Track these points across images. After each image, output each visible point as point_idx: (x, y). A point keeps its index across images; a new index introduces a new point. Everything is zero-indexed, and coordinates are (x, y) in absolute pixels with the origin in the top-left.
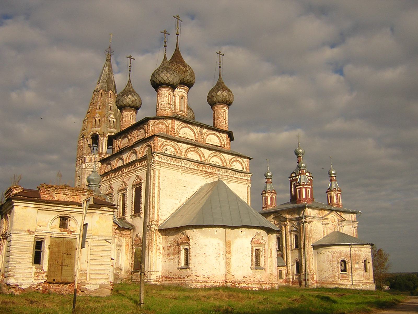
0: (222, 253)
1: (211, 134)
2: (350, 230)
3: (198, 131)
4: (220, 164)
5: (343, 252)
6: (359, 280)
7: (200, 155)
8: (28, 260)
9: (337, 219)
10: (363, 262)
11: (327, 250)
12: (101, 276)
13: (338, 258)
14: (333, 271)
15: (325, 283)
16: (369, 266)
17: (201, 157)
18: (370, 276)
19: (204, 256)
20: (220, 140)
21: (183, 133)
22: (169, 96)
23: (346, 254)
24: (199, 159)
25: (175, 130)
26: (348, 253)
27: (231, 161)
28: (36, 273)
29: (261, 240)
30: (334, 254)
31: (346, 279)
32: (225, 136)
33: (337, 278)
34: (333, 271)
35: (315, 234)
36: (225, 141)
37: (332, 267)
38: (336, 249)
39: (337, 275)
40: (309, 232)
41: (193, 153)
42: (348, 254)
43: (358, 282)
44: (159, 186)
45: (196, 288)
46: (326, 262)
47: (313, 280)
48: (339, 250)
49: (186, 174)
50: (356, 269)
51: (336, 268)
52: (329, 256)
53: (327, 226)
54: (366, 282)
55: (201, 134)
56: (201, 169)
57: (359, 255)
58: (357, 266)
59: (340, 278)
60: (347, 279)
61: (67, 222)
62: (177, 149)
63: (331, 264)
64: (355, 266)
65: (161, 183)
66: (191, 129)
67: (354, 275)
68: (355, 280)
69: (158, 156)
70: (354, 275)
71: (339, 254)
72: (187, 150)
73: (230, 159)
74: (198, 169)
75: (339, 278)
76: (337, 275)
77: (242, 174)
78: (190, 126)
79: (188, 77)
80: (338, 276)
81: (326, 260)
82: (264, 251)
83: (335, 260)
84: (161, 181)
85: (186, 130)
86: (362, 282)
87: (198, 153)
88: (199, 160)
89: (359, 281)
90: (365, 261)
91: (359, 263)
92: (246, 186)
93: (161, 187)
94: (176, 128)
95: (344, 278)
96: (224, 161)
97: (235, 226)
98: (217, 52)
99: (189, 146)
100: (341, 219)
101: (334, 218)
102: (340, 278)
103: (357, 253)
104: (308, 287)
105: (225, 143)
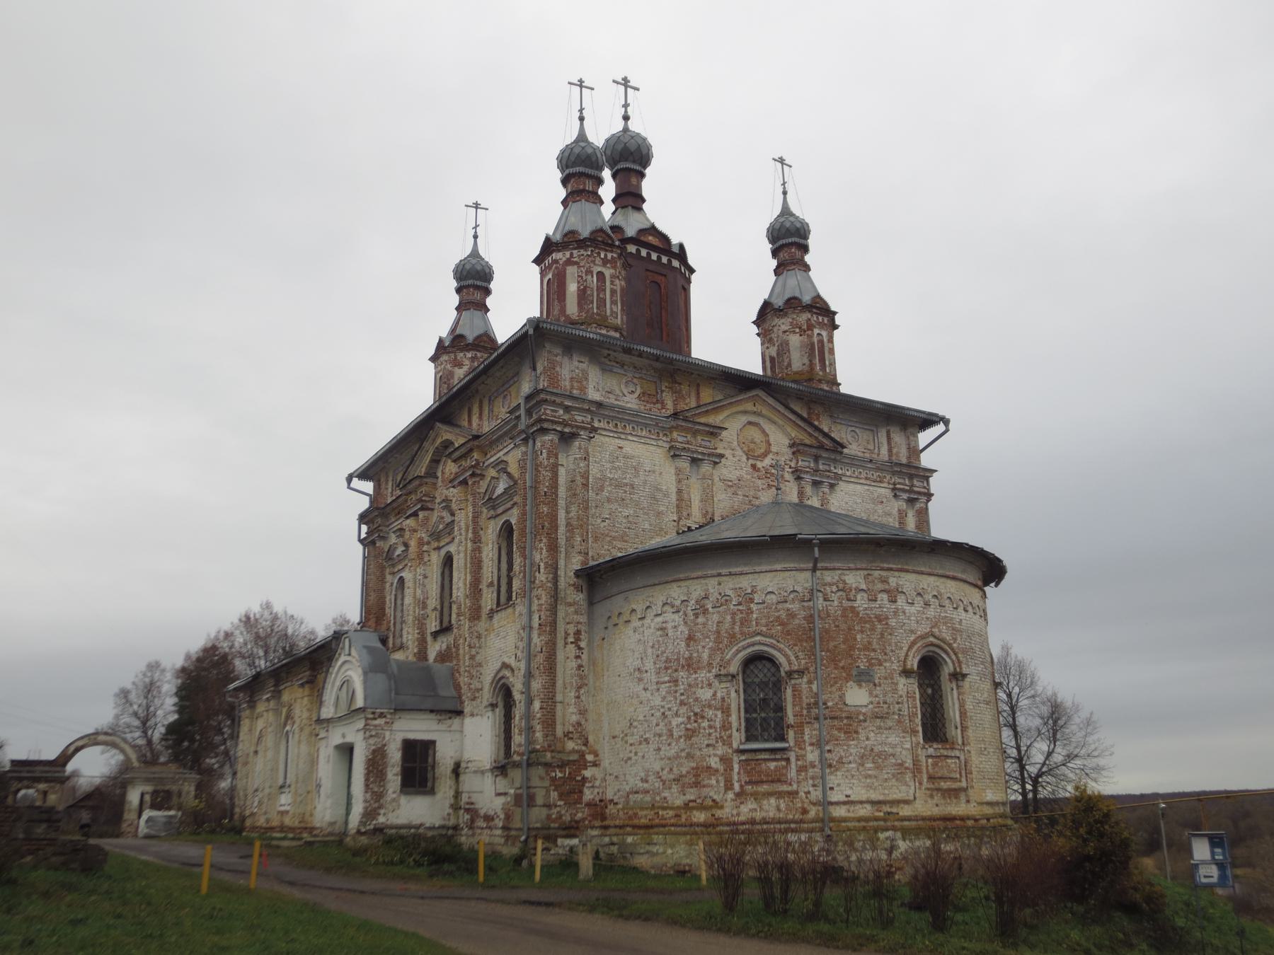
2: (880, 509)
5: (757, 598)
6: (875, 796)
9: (787, 442)
10: (906, 673)
11: (659, 597)
13: (723, 640)
14: (690, 734)
15: (643, 821)
16: (962, 706)
18: (969, 772)
23: (783, 615)
26: (794, 607)
30: (701, 620)
31: (780, 795)
34: (694, 731)
35: (614, 506)
37: (683, 710)
39: (714, 762)
40: (562, 492)
42: (792, 615)
43: (865, 811)
47: (579, 801)
48: (729, 586)
50: (849, 723)
51: (710, 713)
52: (670, 633)
54: (936, 811)
57: (880, 619)
58: (857, 697)
59: (737, 787)
60: (785, 788)
61: (391, 827)
63: (681, 688)
64: (842, 697)
67: (840, 761)
70: (840, 761)
71: (734, 614)
75: (729, 786)
77: (1013, 740)
80: (721, 768)
81: (649, 665)
83: (705, 656)
86: (905, 811)
89: (873, 803)
90: (929, 668)
91: (879, 673)
95: (764, 788)
100: (814, 442)
101: (764, 432)
102: (737, 787)
103: (861, 602)
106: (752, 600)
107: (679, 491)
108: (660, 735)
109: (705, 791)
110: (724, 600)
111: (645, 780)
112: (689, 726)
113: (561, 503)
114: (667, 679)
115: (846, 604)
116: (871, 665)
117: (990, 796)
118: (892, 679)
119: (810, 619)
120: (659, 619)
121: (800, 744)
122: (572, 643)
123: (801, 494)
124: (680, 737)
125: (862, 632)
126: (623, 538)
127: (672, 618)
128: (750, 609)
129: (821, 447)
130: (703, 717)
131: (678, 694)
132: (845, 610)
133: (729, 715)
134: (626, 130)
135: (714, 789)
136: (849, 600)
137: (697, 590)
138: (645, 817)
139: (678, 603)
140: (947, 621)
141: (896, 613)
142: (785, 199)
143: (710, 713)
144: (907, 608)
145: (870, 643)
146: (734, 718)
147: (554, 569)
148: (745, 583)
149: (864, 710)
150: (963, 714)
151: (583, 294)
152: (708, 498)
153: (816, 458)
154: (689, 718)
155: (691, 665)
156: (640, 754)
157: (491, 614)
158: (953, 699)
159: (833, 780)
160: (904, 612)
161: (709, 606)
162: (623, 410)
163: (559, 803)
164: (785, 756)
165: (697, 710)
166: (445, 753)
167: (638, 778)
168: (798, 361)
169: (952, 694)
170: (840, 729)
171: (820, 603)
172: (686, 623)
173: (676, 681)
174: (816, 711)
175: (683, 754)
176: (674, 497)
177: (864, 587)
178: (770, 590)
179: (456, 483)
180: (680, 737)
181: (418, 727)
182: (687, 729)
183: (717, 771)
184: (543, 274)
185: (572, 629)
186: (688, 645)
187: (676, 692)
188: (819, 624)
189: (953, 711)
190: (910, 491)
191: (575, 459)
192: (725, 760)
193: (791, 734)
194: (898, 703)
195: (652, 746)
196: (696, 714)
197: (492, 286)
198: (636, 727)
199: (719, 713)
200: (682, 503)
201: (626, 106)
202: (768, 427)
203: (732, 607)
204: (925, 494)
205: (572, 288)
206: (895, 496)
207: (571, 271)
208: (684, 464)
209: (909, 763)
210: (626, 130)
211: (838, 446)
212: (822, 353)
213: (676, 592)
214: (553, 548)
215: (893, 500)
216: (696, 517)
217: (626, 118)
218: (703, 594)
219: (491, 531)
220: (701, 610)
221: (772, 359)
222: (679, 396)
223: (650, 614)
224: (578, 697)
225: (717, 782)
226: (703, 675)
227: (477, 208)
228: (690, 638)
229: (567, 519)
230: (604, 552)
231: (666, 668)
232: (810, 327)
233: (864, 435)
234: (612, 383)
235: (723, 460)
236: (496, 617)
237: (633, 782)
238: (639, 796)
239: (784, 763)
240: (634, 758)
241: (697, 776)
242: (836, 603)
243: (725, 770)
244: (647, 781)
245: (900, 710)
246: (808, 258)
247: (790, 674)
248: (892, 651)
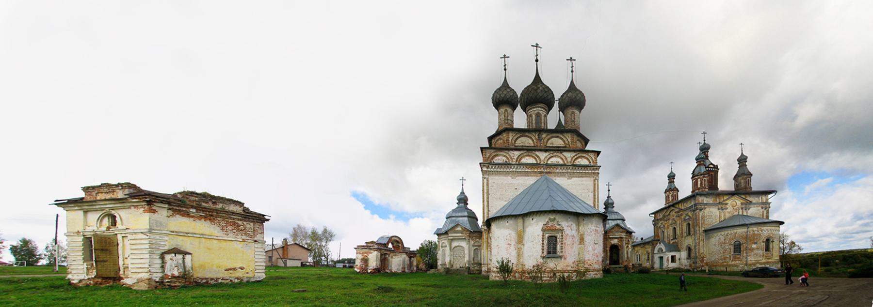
0: (513, 243)
1: (552, 137)
2: (758, 211)
3: (537, 137)
4: (561, 162)
6: (756, 260)
7: (535, 158)
8: (79, 258)
10: (763, 242)
11: (719, 234)
12: (141, 270)
14: (724, 253)
17: (536, 160)
19: (497, 248)
20: (564, 142)
21: (520, 142)
22: (506, 112)
24: (535, 162)
25: (510, 141)
27: (574, 159)
28: (88, 269)
29: (556, 225)
32: (570, 136)
33: (728, 260)
36: (570, 141)
38: (729, 232)
39: (728, 256)
40: (700, 218)
41: (527, 158)
43: (754, 262)
44: (483, 192)
45: (644, 271)
46: (717, 246)
48: (732, 232)
49: (517, 178)
50: (752, 250)
53: (724, 210)
55: (540, 139)
56: (536, 170)
58: (754, 246)
62: (508, 157)
65: (490, 190)
66: (529, 137)
67: (750, 255)
68: (751, 261)
69: (485, 166)
72: (519, 156)
73: (572, 156)
74: (532, 170)
75: (730, 259)
76: (728, 256)
78: (527, 134)
79: (540, 94)
82: (561, 237)
84: (490, 188)
85: (523, 139)
87: (533, 157)
88: (535, 162)
90: (768, 240)
91: (758, 242)
92: (593, 179)
93: (490, 193)
94: (510, 139)
96: (564, 159)
97: (523, 214)
98: (533, 45)
99: (522, 152)
103: (756, 232)
104: (488, 277)
105: (570, 143)
117: (776, 258)
119: (747, 235)
121: (743, 253)
123: (742, 212)
126: (710, 224)
127: (721, 237)
129: (747, 203)
134: (705, 143)
135: (728, 260)
137: (726, 232)
138: (715, 264)
146: (732, 250)
147: (699, 230)
148: (735, 231)
150: (773, 247)
151: (701, 183)
152: (725, 215)
153: (746, 205)
155: (724, 243)
157: (685, 237)
159: (748, 258)
162: (710, 204)
166: (677, 257)
168: (743, 185)
171: (749, 233)
173: (722, 246)
174: (747, 249)
176: (719, 216)
181: (673, 254)
184: (693, 181)
188: (748, 236)
189: (771, 246)
192: (730, 256)
193: (742, 252)
200: (720, 217)
201: (704, 138)
202: (736, 201)
204: (750, 175)
205: (699, 183)
207: (699, 180)
209: (762, 255)
210: (705, 143)
211: (751, 202)
212: (748, 182)
213: (723, 233)
214: (699, 227)
216: (723, 219)
217: (704, 140)
219: (685, 225)
221: (737, 185)
222: (720, 199)
226: (727, 245)
227: (537, 47)
228: (725, 239)
230: (707, 227)
232: (746, 178)
233: (756, 199)
234: (708, 199)
236: (687, 238)
246: (746, 163)
247: (742, 244)
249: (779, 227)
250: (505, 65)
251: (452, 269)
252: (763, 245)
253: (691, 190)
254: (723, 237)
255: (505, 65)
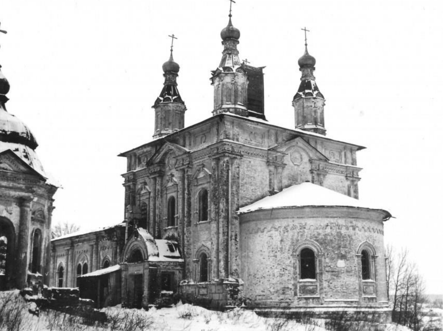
14: (281, 275)
26: (320, 231)
30: (286, 234)
34: (283, 275)
39: (290, 286)
40: (230, 181)
42: (319, 234)
46: (266, 254)
48: (297, 222)
50: (336, 273)
58: (341, 264)
75: (295, 294)
81: (265, 249)
103: (343, 231)
106: (305, 228)
107: (270, 180)
108: (270, 275)
109: (287, 296)
110: (294, 228)
111: (263, 291)
112: (281, 273)
113: (230, 184)
114: (273, 255)
115: (338, 230)
116: (346, 253)
118: (353, 258)
120: (269, 233)
122: (234, 239)
124: (278, 276)
125: (343, 241)
127: (274, 232)
128: (304, 231)
130: (286, 270)
131: (277, 261)
132: (338, 233)
133: (296, 269)
136: (339, 229)
139: (277, 227)
140: (371, 237)
141: (355, 234)
142: (306, 48)
143: (289, 268)
144: (359, 232)
145: (346, 245)
149: (343, 269)
150: (376, 271)
154: (281, 270)
156: (261, 282)
158: (372, 265)
160: (358, 234)
161: (289, 229)
163: (230, 299)
164: (315, 285)
165: (284, 267)
167: (260, 291)
169: (372, 263)
170: (335, 275)
172: (280, 235)
173: (276, 256)
175: (279, 283)
177: (344, 224)
178: (312, 224)
179: (179, 169)
180: (278, 276)
182: (280, 274)
183: (291, 289)
185: (234, 234)
186: (281, 243)
187: (276, 260)
190: (353, 177)
191: (235, 167)
194: (354, 267)
195: (266, 280)
196: (284, 269)
197: (179, 73)
198: (260, 272)
199: (292, 269)
203: (297, 230)
206: (347, 179)
208: (272, 168)
209: (358, 288)
214: (227, 202)
215: (346, 181)
218: (287, 225)
220: (286, 229)
223: (266, 230)
224: (236, 260)
225: (291, 293)
227: (173, 37)
228: (282, 241)
229: (232, 191)
231: (273, 251)
235: (286, 166)
237: (258, 292)
238: (260, 297)
239: (315, 287)
240: (259, 283)
241: (283, 290)
242: (335, 230)
243: (295, 289)
244: (264, 292)
245: (355, 269)
248: (353, 248)
249: (383, 224)
250: (172, 47)
251: (64, 313)
252: (356, 263)
253: (212, 109)
254: (277, 233)
255: (172, 47)
